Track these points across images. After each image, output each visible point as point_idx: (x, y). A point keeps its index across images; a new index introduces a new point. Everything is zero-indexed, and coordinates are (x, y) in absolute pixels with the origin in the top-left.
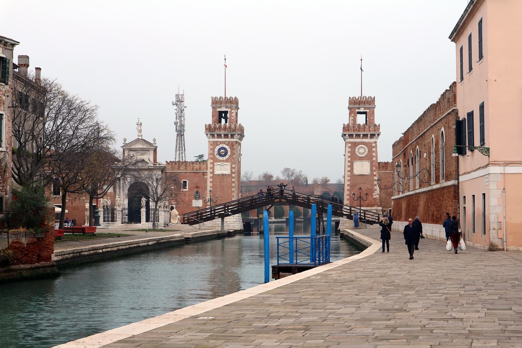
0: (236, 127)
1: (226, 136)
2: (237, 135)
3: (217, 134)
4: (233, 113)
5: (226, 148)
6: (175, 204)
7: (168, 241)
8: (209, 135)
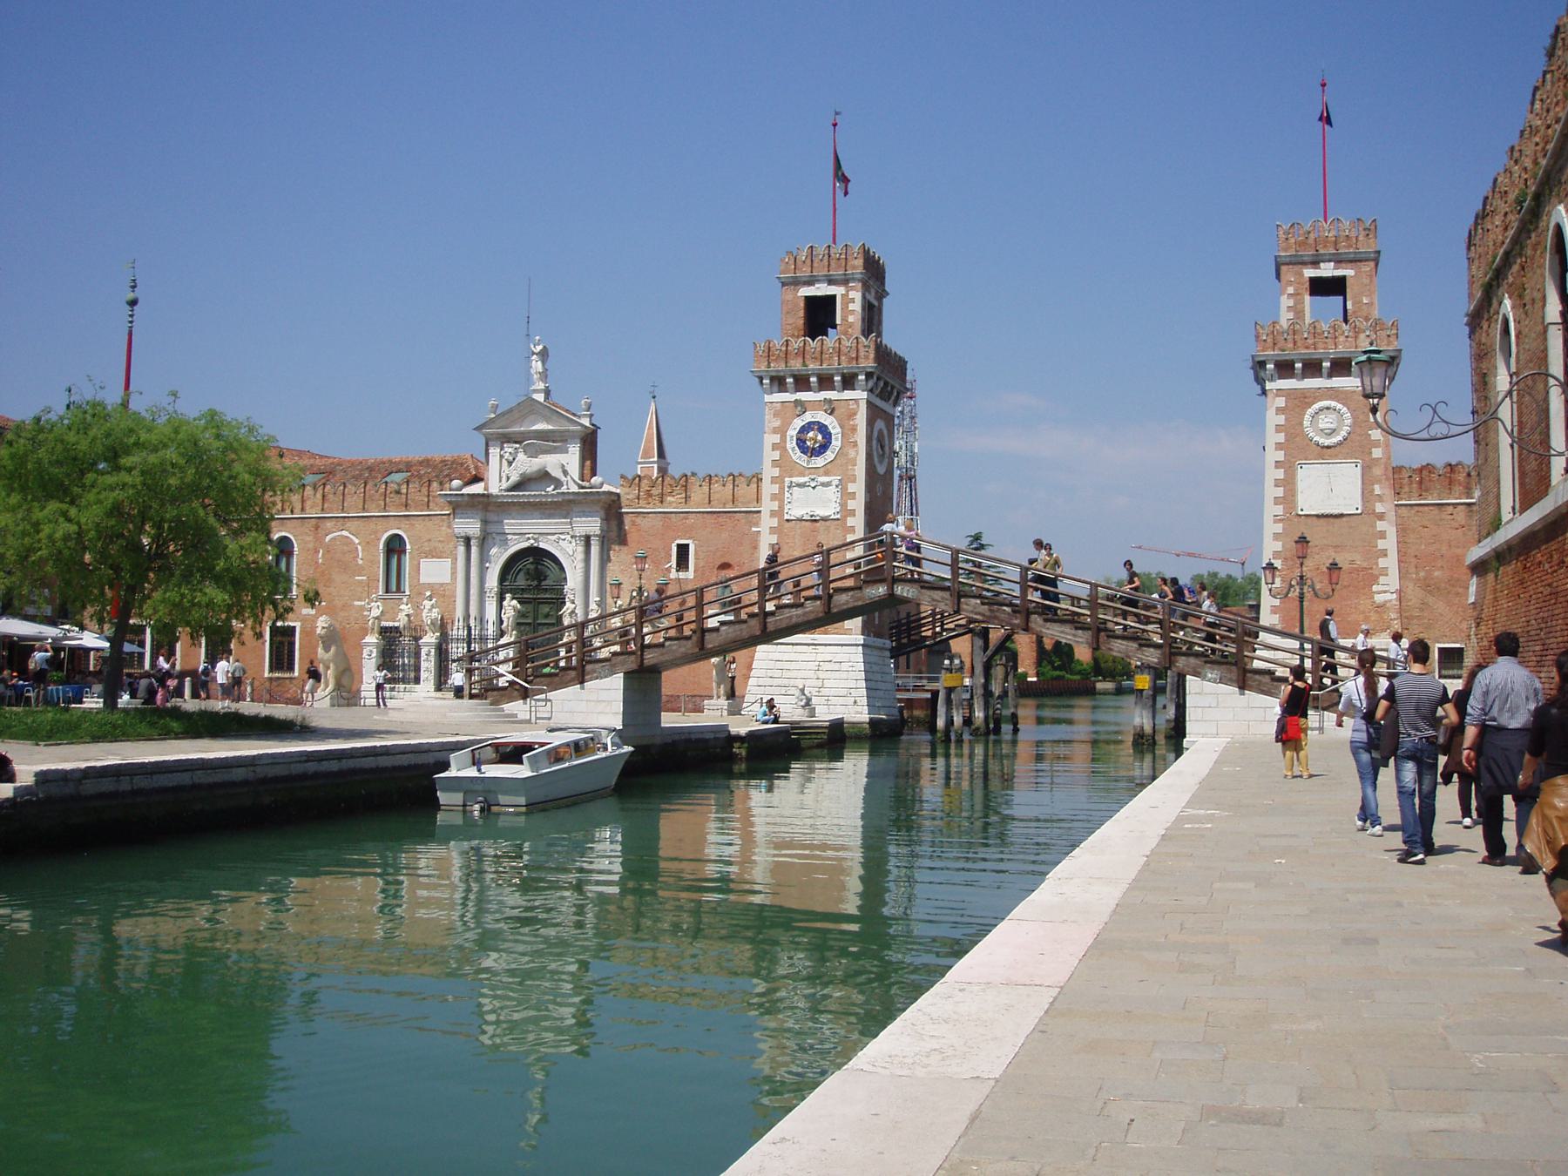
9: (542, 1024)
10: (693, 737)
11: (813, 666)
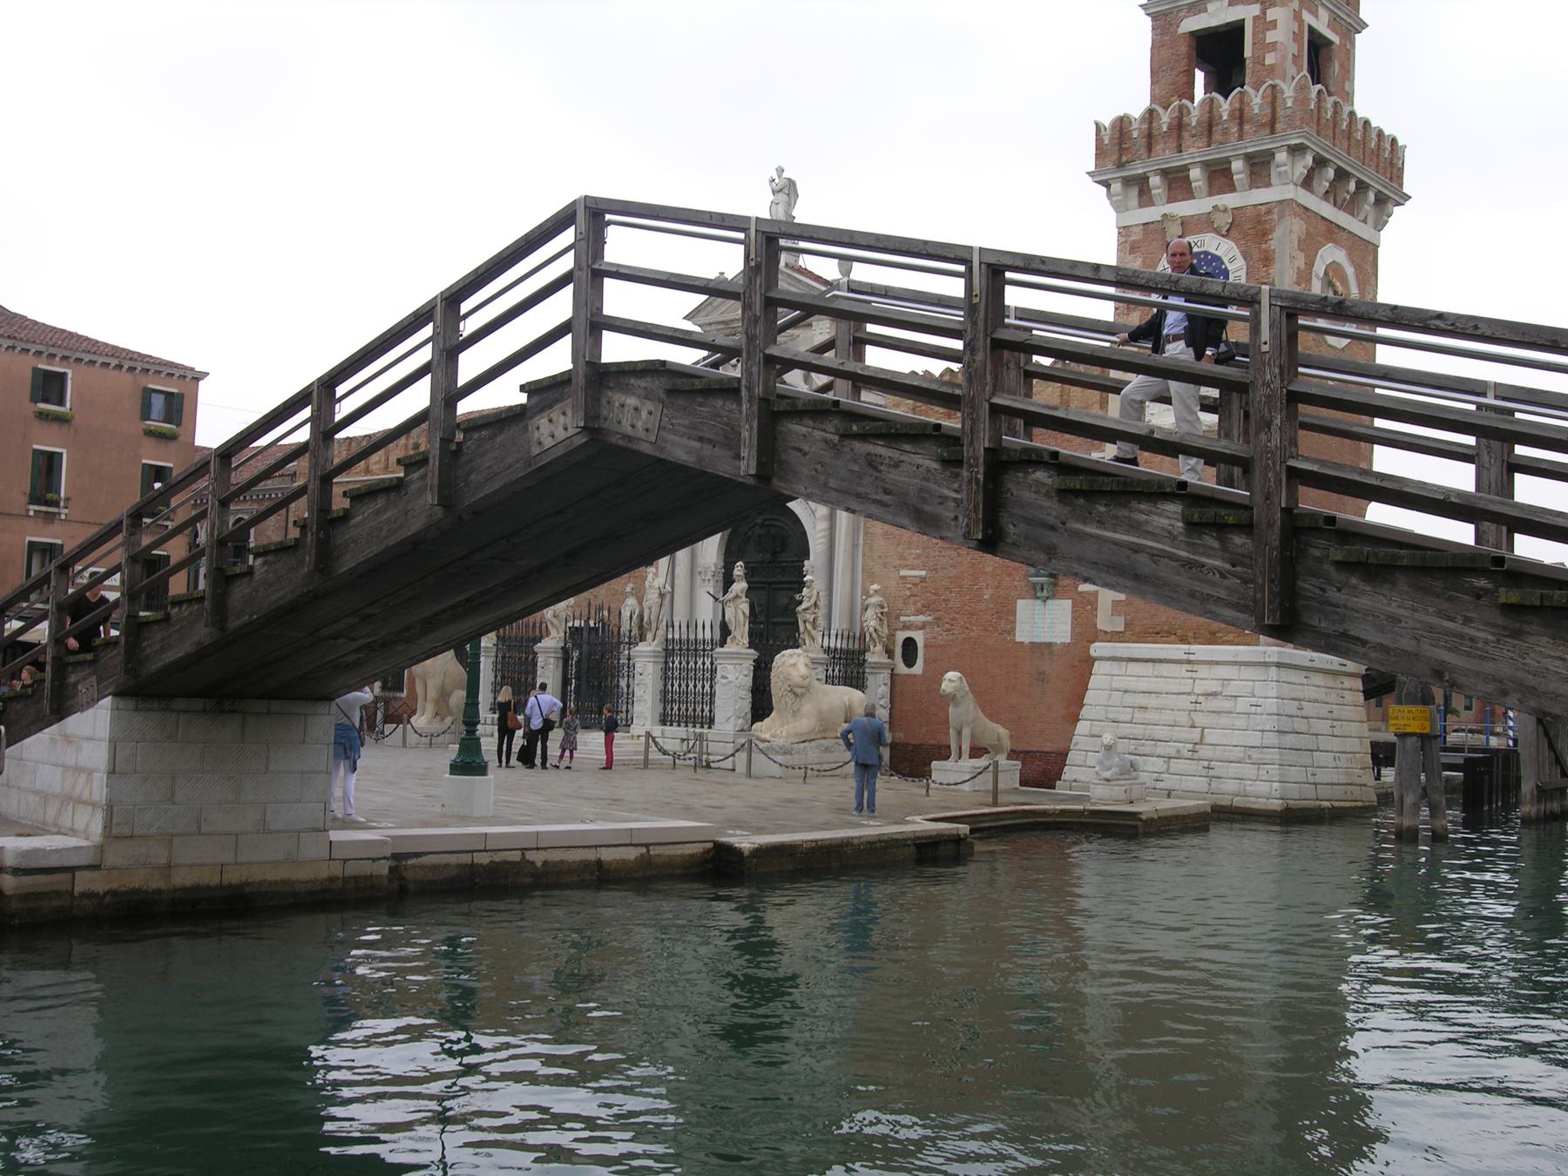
0: (1279, 101)
1: (1219, 176)
2: (1281, 157)
3: (1165, 173)
4: (1274, 24)
5: (1218, 259)
6: (923, 627)
7: (758, 942)
8: (1117, 187)
9: (1084, 1149)
10: (537, 858)
11: (1184, 702)
